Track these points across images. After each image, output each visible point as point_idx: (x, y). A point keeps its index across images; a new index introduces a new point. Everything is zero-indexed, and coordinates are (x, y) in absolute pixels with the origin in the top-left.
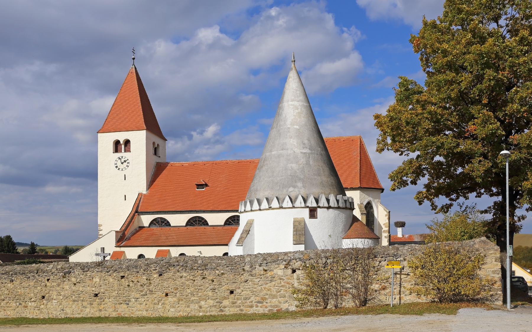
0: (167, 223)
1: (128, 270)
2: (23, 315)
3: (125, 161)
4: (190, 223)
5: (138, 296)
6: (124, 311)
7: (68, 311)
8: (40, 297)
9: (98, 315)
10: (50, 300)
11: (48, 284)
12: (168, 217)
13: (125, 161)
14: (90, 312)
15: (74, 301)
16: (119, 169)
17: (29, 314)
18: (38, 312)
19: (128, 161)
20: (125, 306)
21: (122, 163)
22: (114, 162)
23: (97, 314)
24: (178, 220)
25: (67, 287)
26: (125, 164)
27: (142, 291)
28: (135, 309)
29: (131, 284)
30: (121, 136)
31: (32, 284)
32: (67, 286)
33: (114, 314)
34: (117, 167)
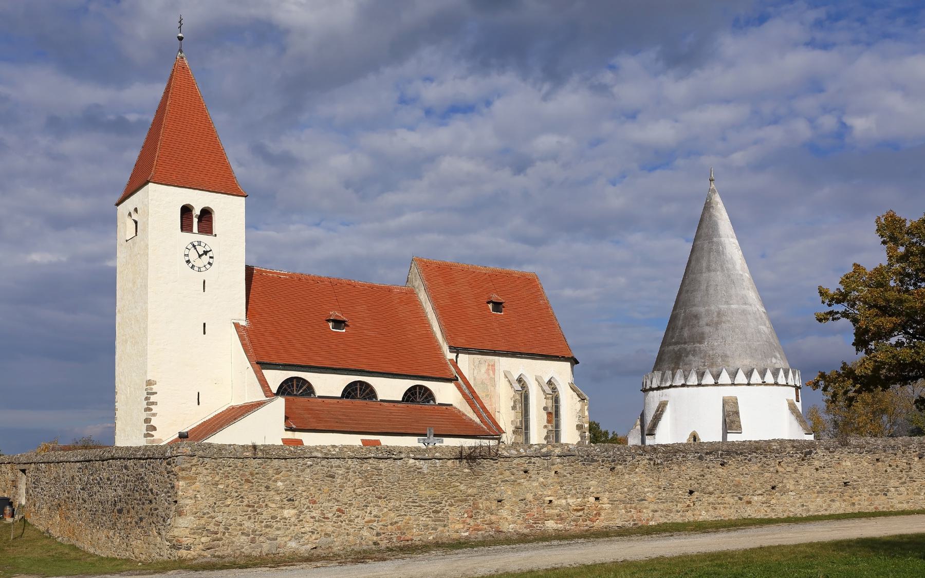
0: (308, 389)
1: (885, 451)
2: (746, 515)
3: (206, 253)
4: (350, 391)
5: (897, 484)
6: (881, 503)
7: (812, 507)
8: (769, 487)
9: (851, 511)
10: (784, 492)
11: (780, 469)
12: (311, 377)
13: (206, 253)
14: (839, 507)
15: (818, 492)
16: (193, 267)
17: (749, 512)
18: (769, 510)
19: (210, 254)
20: (884, 497)
21: (200, 256)
22: (183, 251)
23: (850, 510)
24: (390, 389)
25: (807, 474)
26: (205, 259)
27: (900, 478)
28: (895, 501)
29: (889, 469)
30: (199, 200)
31: (755, 468)
32: (806, 470)
33: (871, 509)
34: (188, 262)
